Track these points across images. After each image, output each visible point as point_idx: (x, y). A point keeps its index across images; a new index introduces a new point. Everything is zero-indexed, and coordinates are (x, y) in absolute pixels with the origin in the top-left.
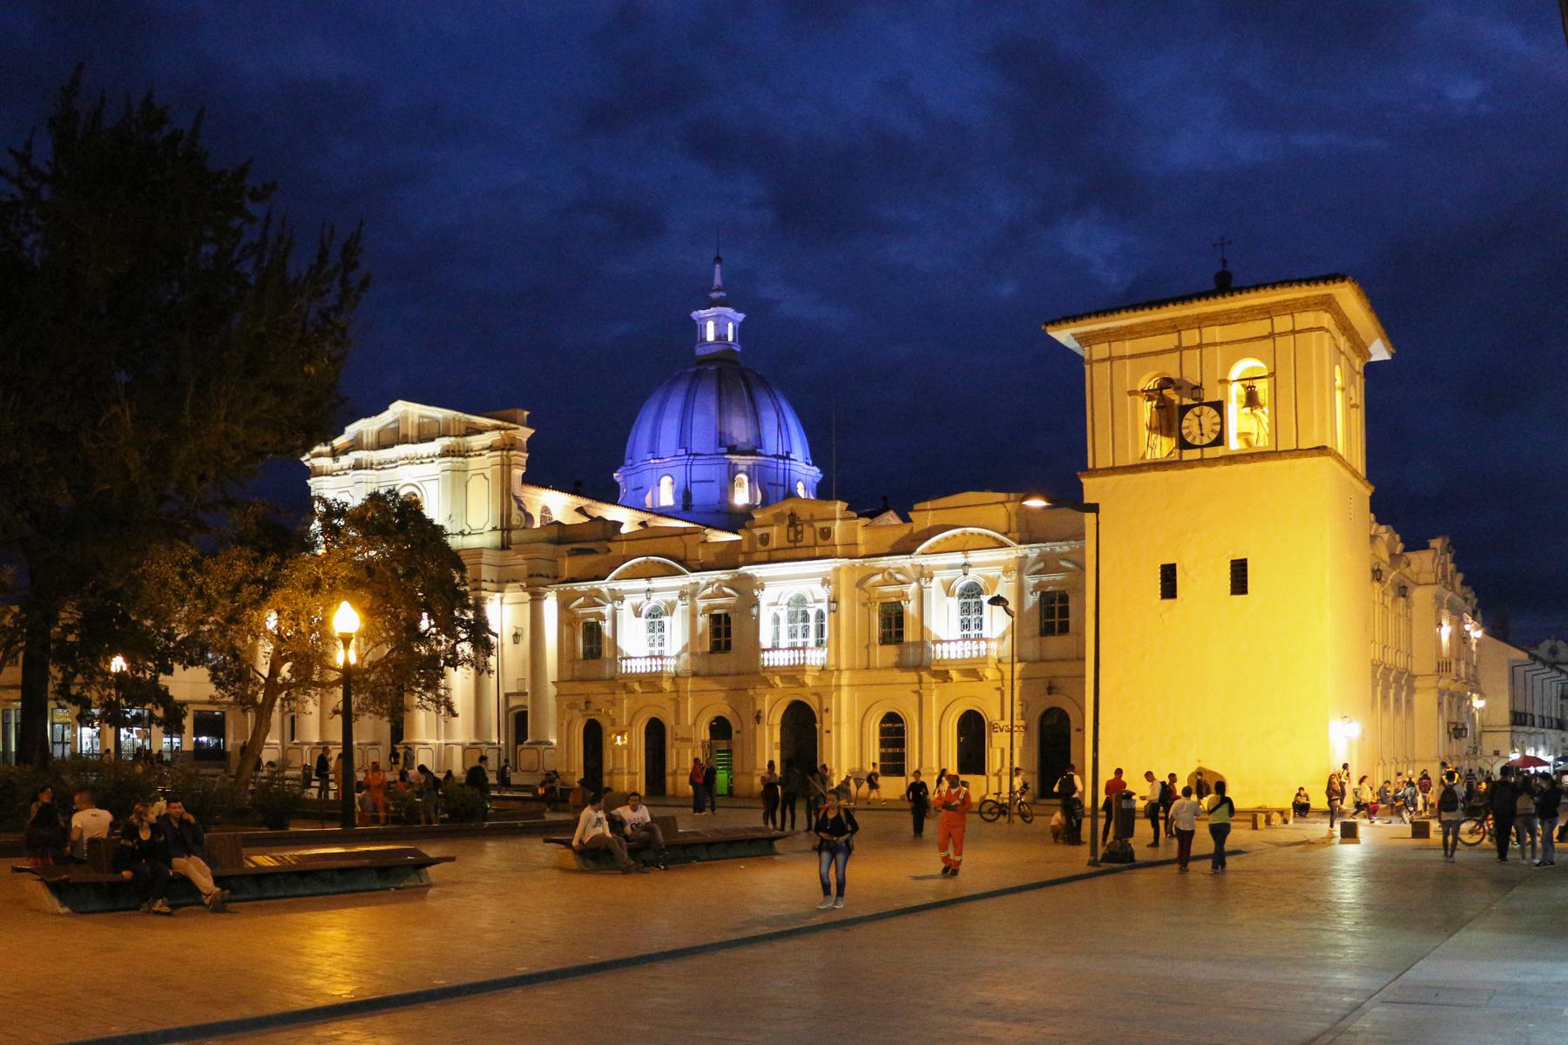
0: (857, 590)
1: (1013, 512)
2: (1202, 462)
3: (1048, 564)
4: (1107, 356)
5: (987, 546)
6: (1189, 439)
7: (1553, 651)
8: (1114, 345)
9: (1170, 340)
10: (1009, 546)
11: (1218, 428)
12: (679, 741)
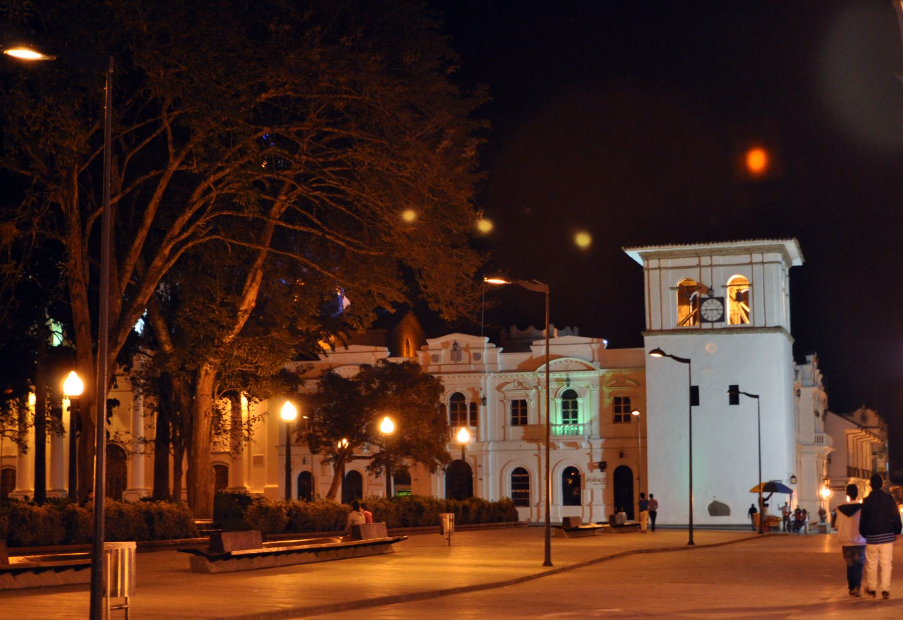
0: (496, 391)
1: (596, 349)
2: (713, 330)
3: (618, 381)
4: (657, 266)
5: (576, 369)
6: (705, 317)
7: (864, 418)
8: (662, 261)
9: (694, 261)
10: (594, 370)
11: (721, 312)
12: (372, 486)
